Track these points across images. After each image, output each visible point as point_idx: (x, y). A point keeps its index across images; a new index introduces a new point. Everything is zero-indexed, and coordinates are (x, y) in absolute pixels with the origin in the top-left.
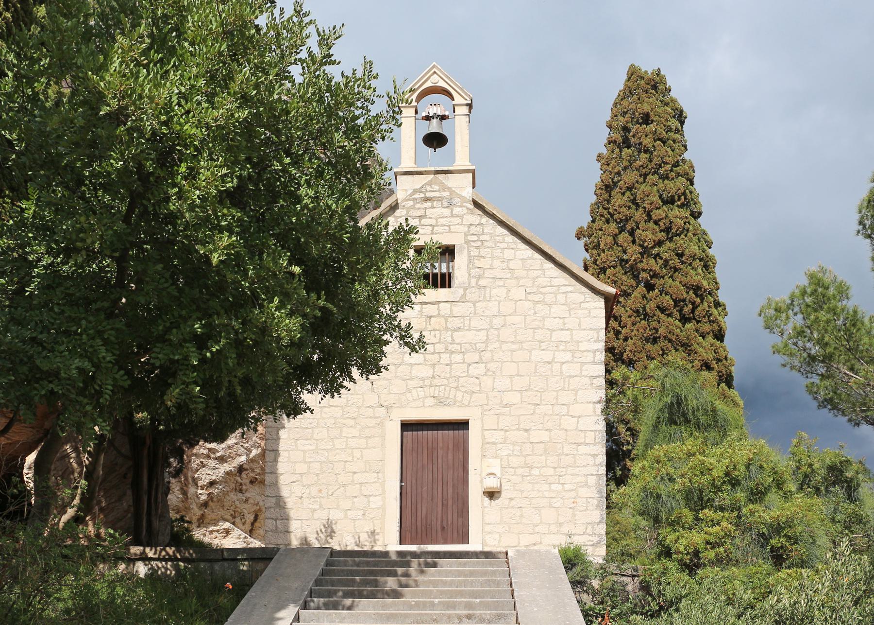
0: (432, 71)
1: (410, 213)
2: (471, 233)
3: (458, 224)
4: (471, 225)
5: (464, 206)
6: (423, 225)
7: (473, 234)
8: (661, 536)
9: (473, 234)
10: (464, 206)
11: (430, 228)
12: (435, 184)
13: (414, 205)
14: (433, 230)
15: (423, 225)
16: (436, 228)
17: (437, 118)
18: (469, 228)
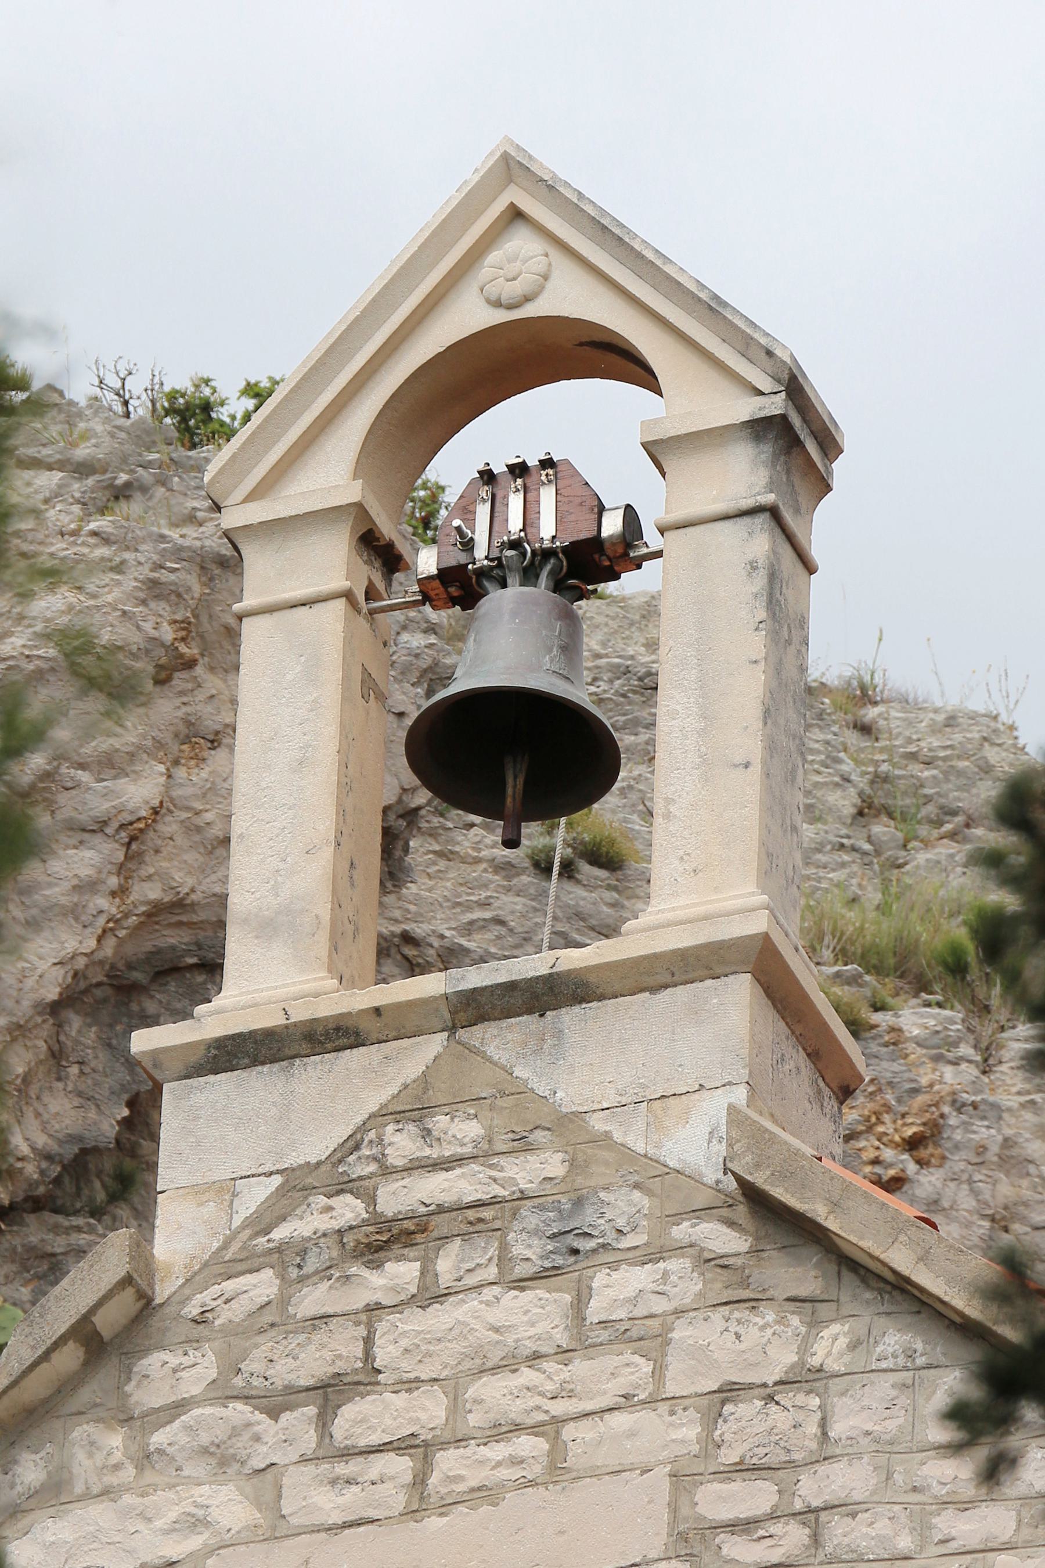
0: (499, 207)
1: (253, 1365)
2: (729, 1456)
3: (627, 1401)
4: (730, 1392)
5: (680, 1249)
6: (347, 1454)
7: (743, 1469)
8: (199, 431)
9: (743, 1469)
10: (680, 1249)
11: (401, 1466)
12: (453, 1107)
13: (284, 1301)
14: (420, 1480)
15: (347, 1454)
16: (447, 1461)
17: (529, 575)
18: (713, 1417)
